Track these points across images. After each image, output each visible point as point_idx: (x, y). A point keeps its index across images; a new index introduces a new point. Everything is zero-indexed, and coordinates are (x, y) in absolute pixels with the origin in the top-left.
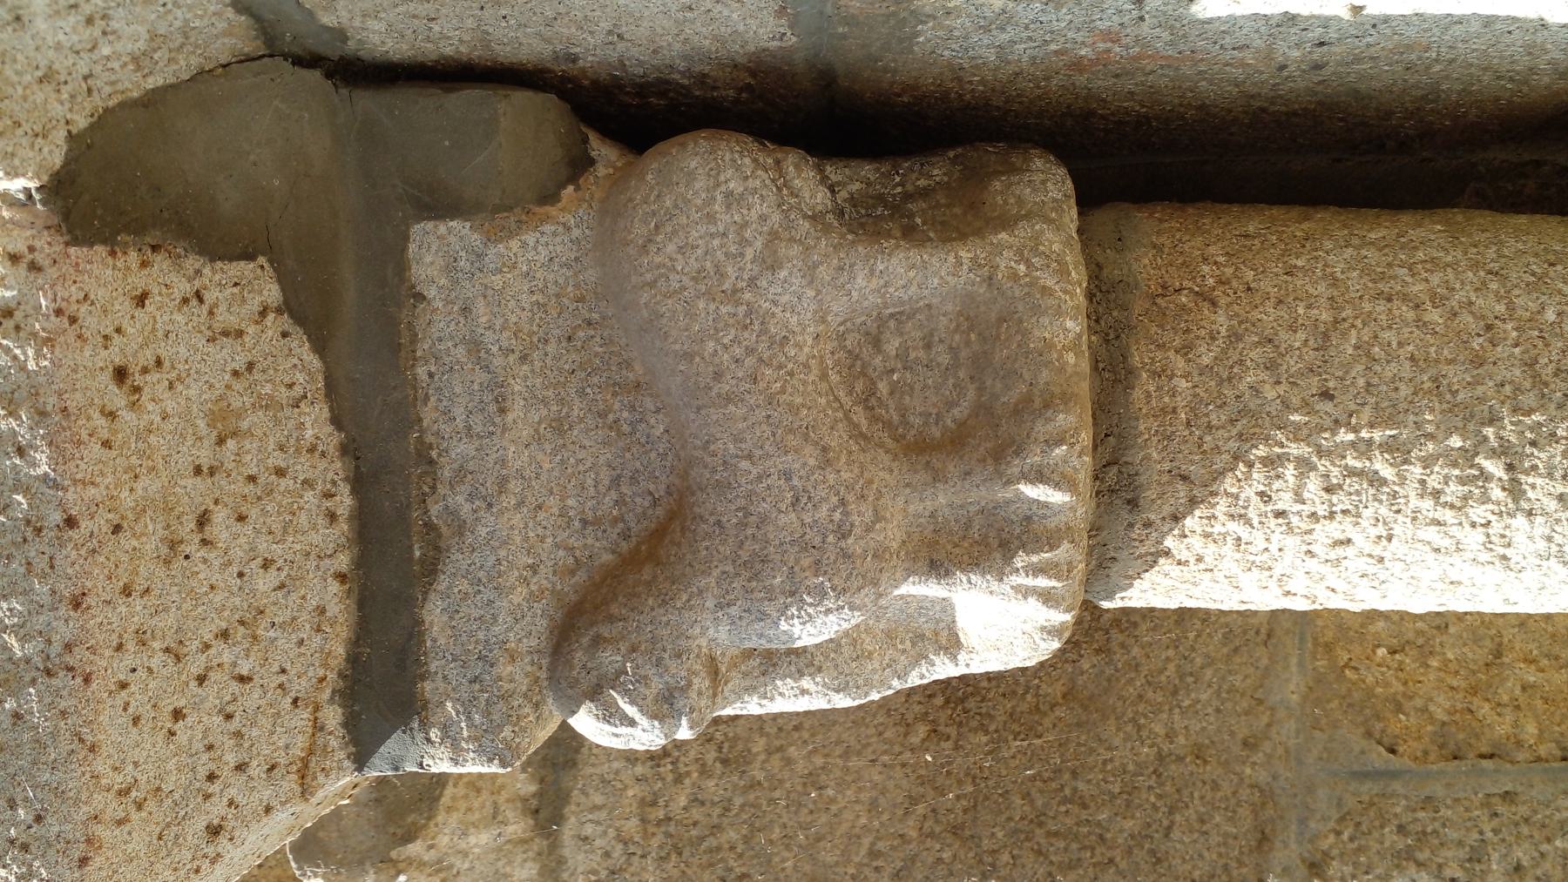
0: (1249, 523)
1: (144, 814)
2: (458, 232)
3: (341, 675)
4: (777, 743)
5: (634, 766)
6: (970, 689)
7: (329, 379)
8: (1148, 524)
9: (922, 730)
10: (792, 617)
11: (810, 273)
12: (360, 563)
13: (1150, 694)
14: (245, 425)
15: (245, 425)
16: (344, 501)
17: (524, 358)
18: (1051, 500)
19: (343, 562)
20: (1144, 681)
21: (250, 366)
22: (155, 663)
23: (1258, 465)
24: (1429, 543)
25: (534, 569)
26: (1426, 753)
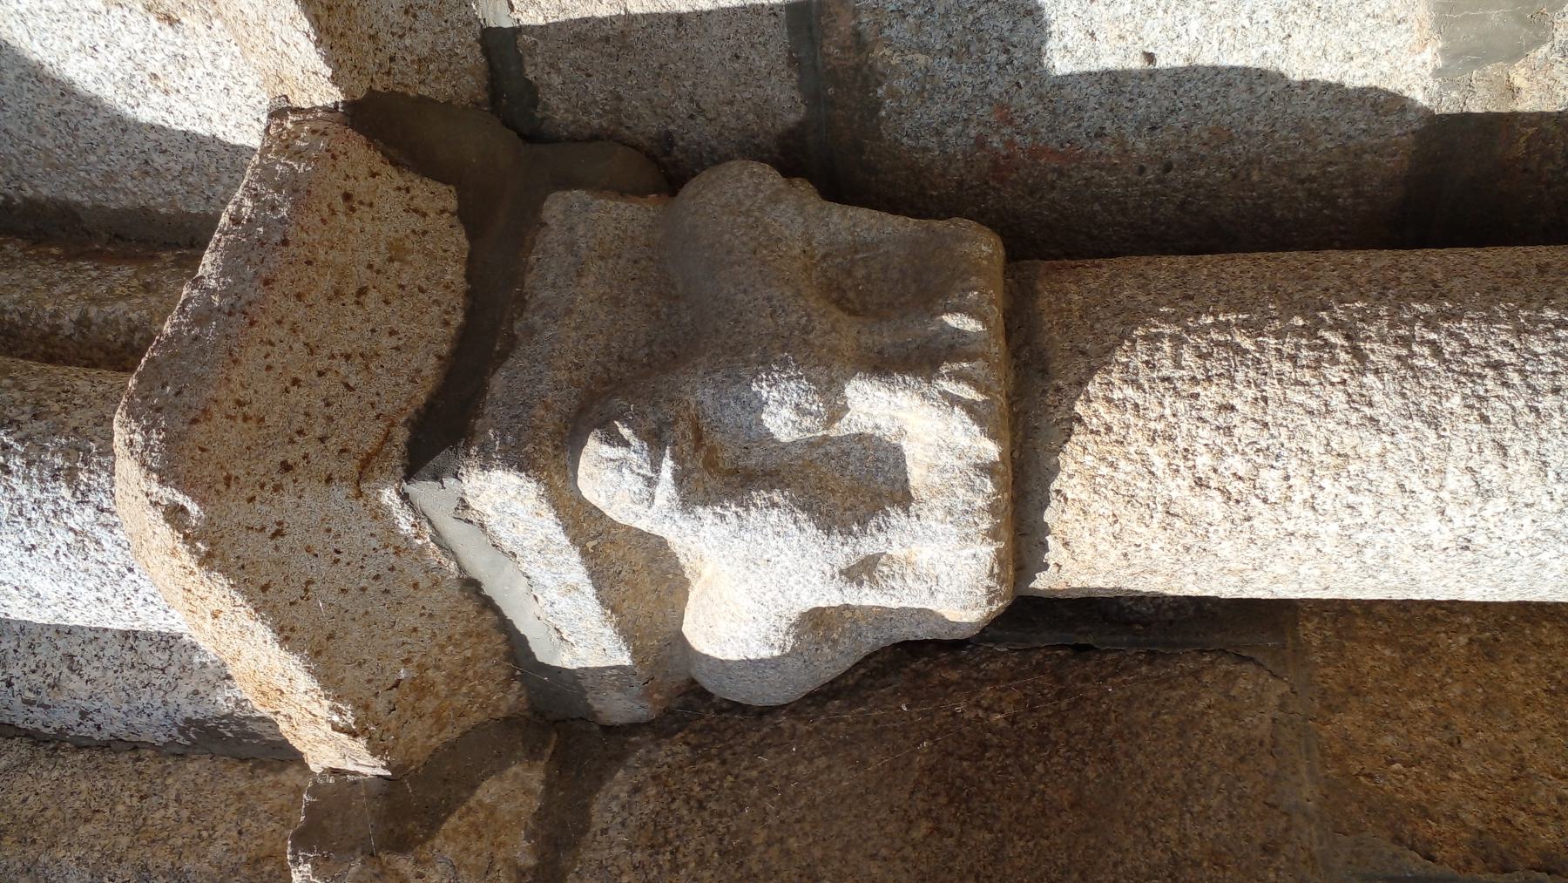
0: (1140, 387)
1: (246, 426)
2: (577, 196)
3: (417, 411)
4: (778, 835)
5: (633, 852)
6: (974, 789)
7: (471, 255)
8: (1058, 389)
9: (924, 826)
10: (762, 380)
11: (801, 210)
12: (455, 353)
13: (1158, 800)
14: (409, 258)
15: (409, 258)
16: (458, 319)
17: (601, 258)
18: (968, 328)
19: (445, 349)
20: (1151, 787)
21: (425, 233)
22: (296, 346)
23: (1139, 340)
24: (1301, 405)
25: (578, 367)
26: (1468, 862)
